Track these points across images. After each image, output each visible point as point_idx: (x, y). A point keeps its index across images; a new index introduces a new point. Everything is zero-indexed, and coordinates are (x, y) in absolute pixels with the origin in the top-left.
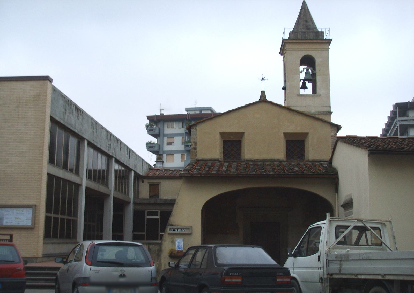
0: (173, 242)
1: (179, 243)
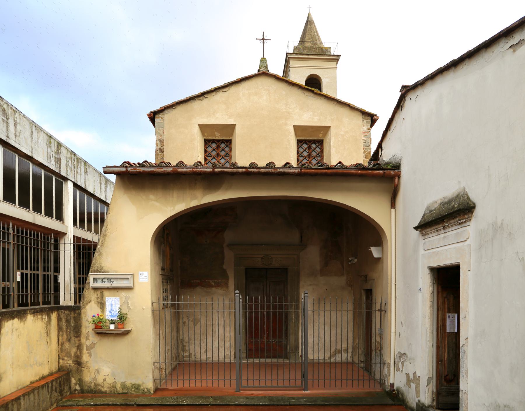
0: (102, 305)
1: (112, 305)
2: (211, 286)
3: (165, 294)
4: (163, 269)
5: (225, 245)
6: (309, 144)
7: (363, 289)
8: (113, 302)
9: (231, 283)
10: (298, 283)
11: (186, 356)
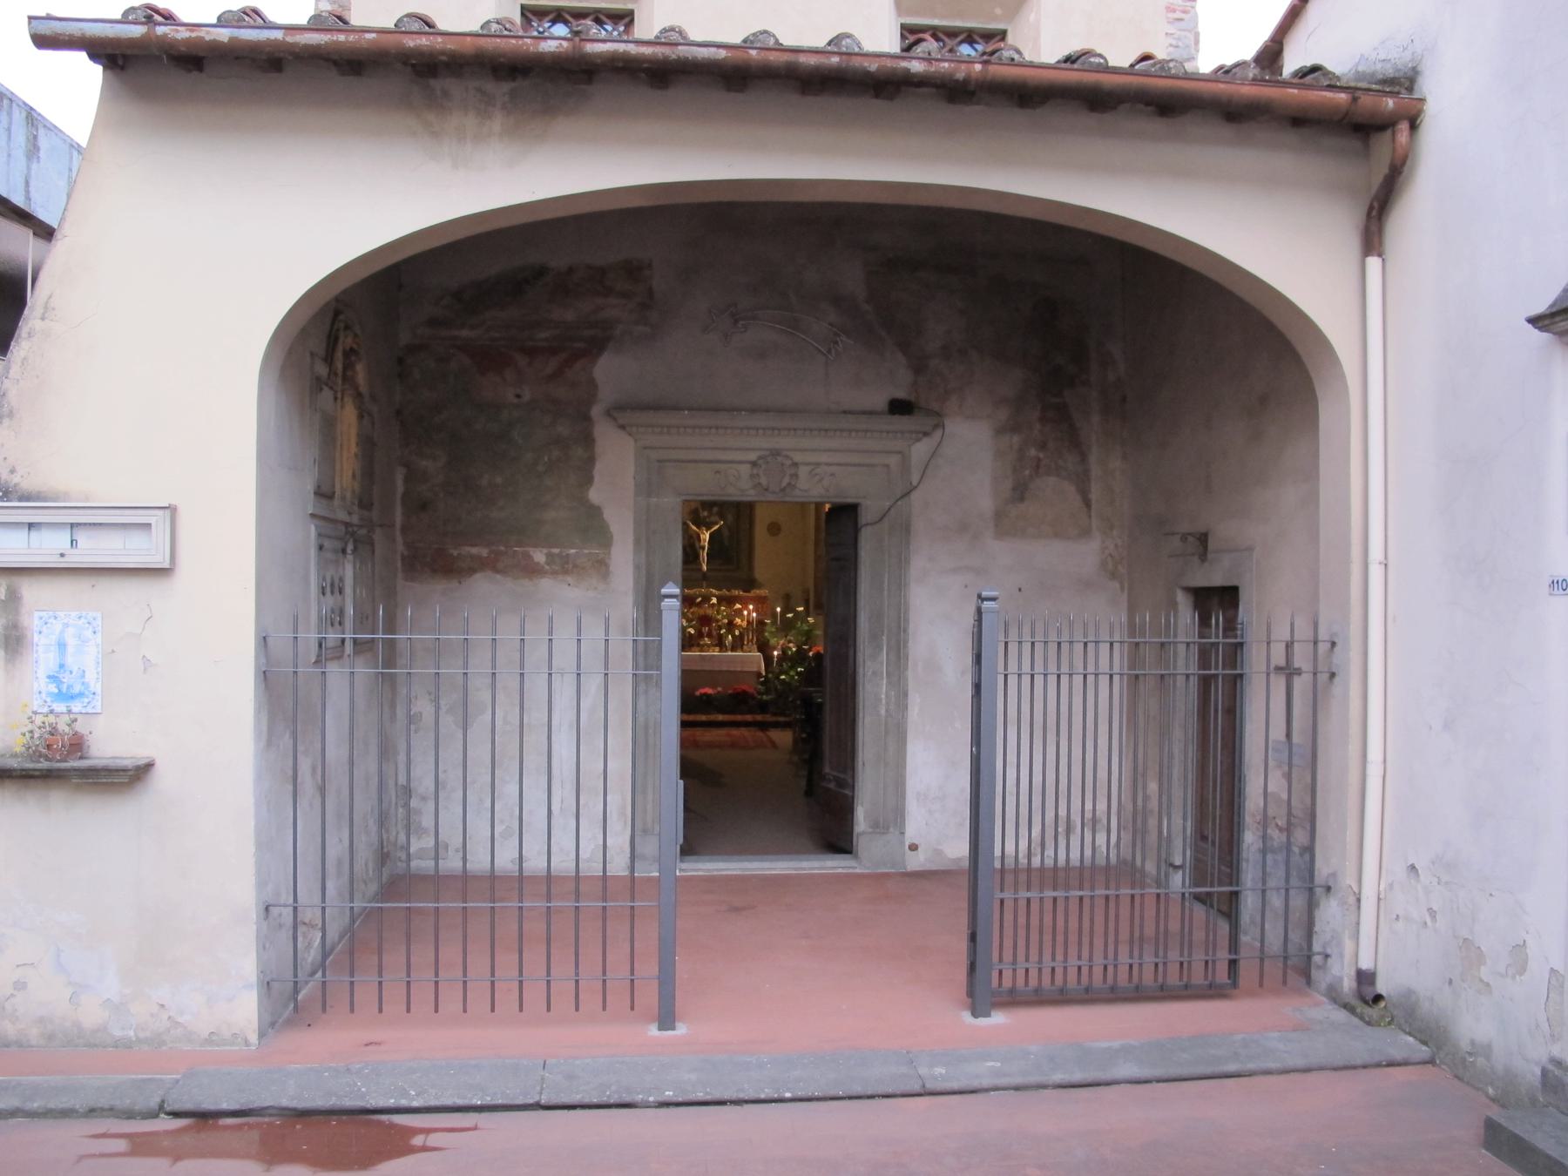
1: (62, 646)
2: (532, 571)
3: (330, 600)
4: (324, 494)
5: (596, 411)
6: (950, 43)
7: (1188, 590)
8: (71, 630)
9: (623, 559)
10: (902, 562)
11: (421, 854)
